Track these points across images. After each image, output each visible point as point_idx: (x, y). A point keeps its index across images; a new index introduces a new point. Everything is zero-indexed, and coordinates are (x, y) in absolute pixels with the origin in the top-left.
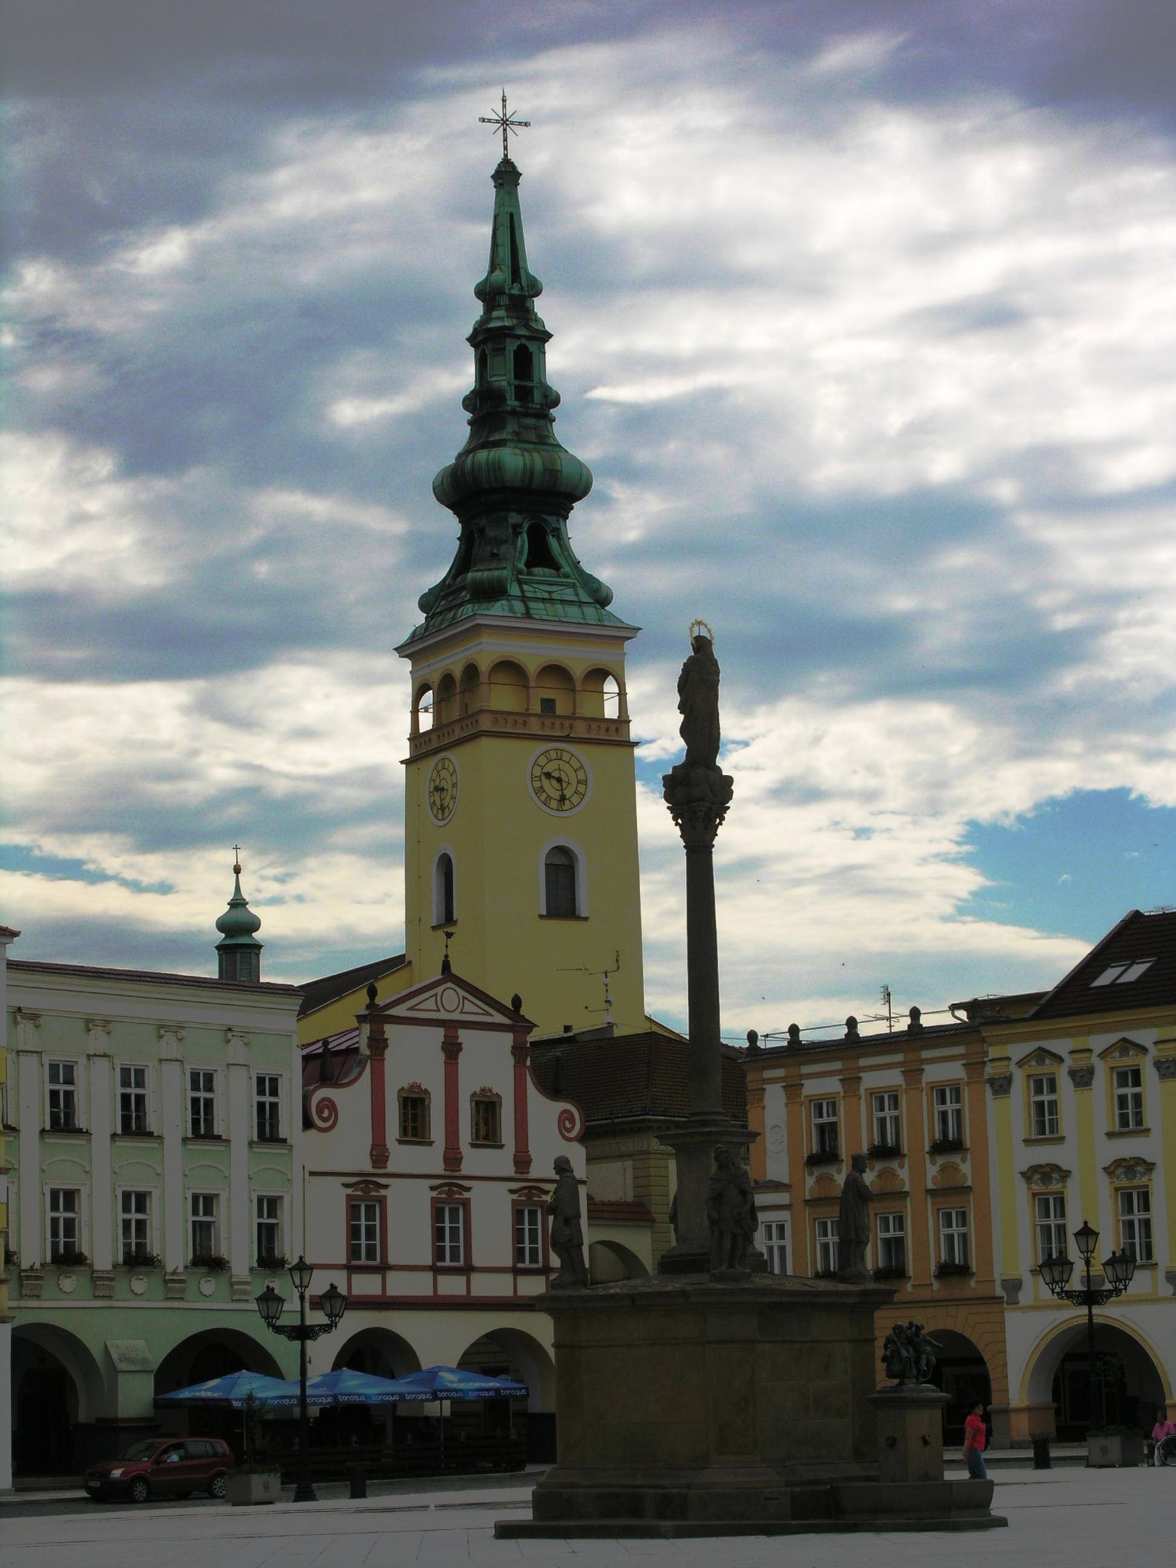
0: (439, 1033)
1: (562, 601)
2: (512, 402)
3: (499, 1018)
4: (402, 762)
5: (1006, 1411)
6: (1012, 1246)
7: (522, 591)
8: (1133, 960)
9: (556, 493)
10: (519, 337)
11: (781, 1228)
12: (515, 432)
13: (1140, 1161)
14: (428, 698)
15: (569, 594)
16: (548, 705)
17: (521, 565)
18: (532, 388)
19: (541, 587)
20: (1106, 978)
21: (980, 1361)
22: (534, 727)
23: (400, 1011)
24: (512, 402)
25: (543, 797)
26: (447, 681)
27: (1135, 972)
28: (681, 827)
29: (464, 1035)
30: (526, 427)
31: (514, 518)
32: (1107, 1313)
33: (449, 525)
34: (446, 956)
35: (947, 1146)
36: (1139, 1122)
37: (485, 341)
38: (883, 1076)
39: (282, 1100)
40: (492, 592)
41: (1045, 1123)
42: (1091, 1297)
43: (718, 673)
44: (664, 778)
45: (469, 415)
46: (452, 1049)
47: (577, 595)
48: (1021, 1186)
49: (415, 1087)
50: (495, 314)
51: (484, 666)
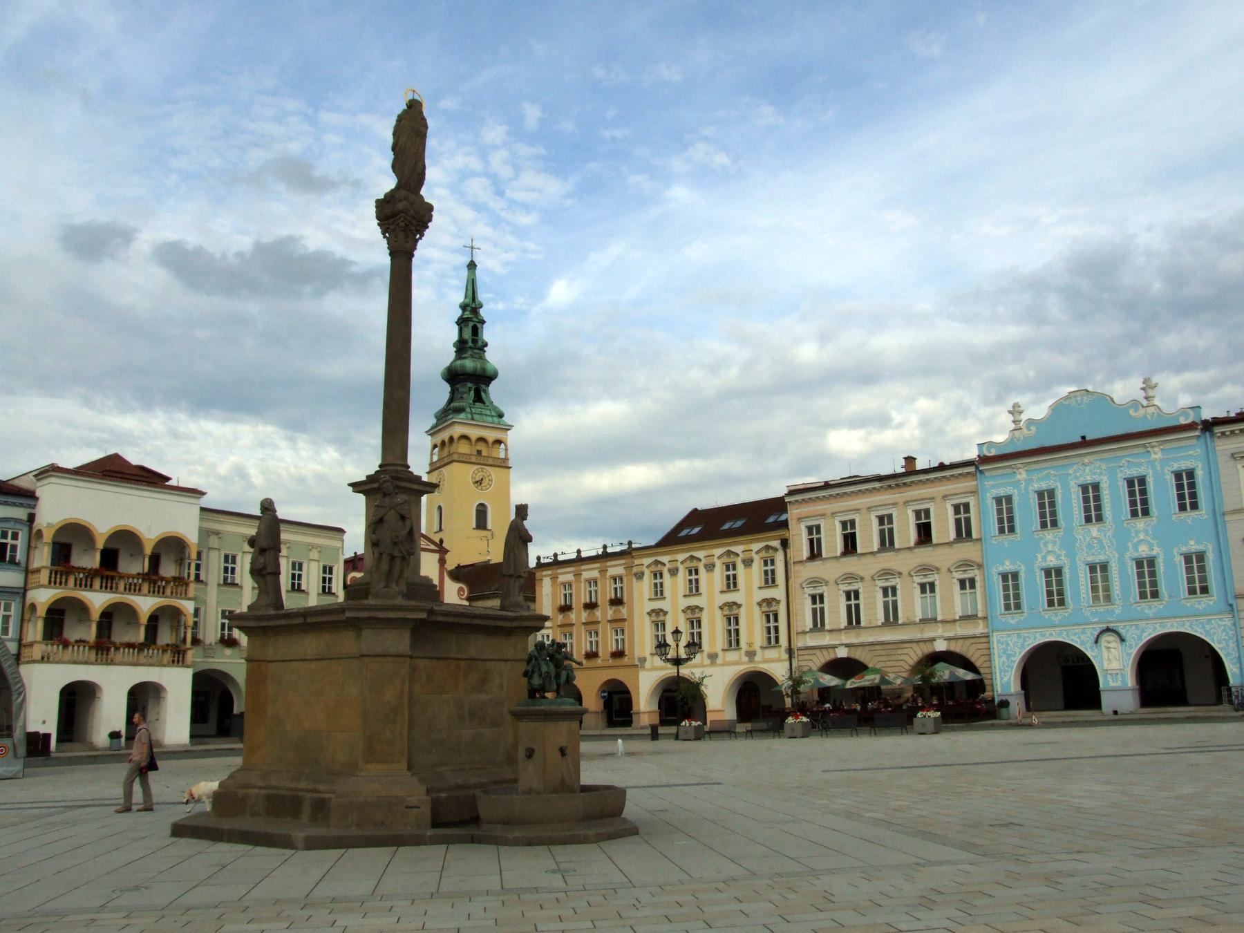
3: (433, 547)
5: (638, 713)
6: (643, 640)
8: (695, 526)
9: (484, 378)
13: (697, 607)
16: (479, 452)
20: (684, 533)
21: (628, 692)
22: (473, 459)
24: (470, 344)
26: (443, 443)
27: (696, 530)
28: (388, 240)
31: (469, 385)
32: (685, 671)
33: (447, 388)
35: (617, 602)
36: (697, 590)
38: (590, 572)
39: (334, 576)
40: (460, 410)
41: (659, 592)
42: (677, 662)
43: (426, 127)
44: (378, 201)
48: (647, 618)
51: (456, 436)
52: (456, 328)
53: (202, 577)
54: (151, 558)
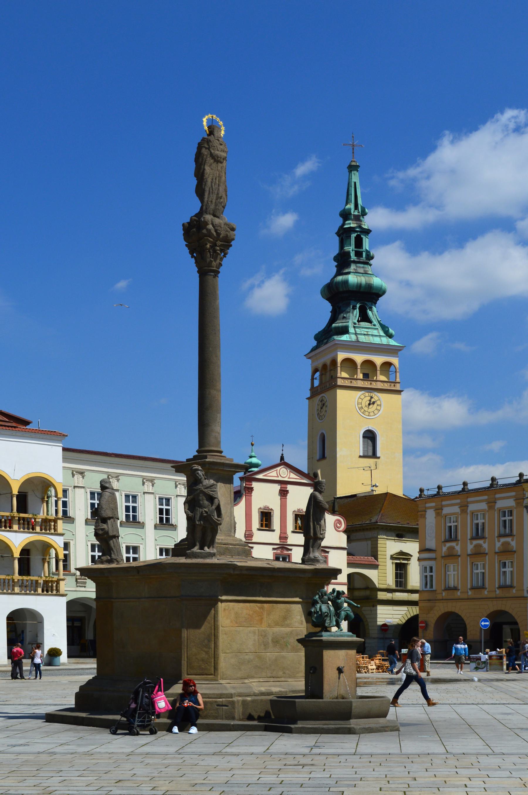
0: (277, 487)
1: (372, 335)
2: (353, 257)
4: (307, 399)
7: (355, 331)
10: (357, 231)
11: (431, 568)
12: (354, 269)
14: (317, 375)
15: (375, 332)
17: (356, 321)
18: (362, 252)
19: (363, 329)
23: (260, 476)
24: (353, 257)
25: (362, 411)
26: (325, 366)
29: (289, 487)
30: (360, 267)
33: (328, 307)
34: (282, 454)
37: (343, 234)
45: (336, 264)
46: (283, 493)
47: (379, 333)
49: (266, 508)
50: (347, 222)
52: (337, 239)
53: (71, 513)
54: (18, 497)
